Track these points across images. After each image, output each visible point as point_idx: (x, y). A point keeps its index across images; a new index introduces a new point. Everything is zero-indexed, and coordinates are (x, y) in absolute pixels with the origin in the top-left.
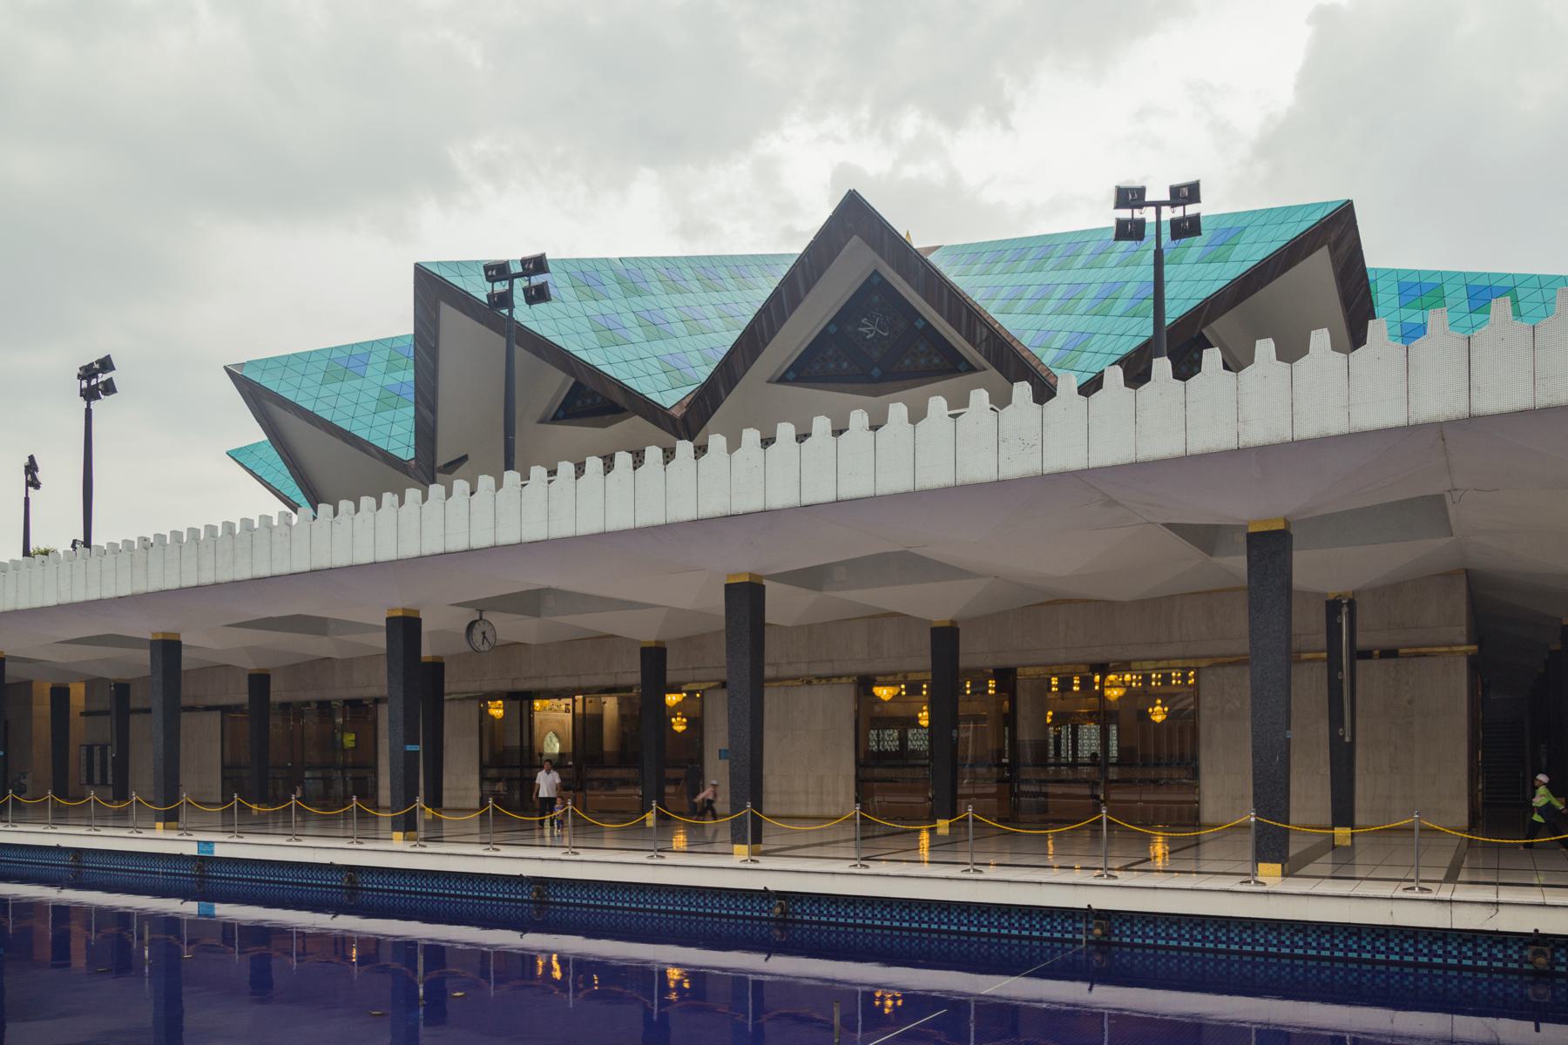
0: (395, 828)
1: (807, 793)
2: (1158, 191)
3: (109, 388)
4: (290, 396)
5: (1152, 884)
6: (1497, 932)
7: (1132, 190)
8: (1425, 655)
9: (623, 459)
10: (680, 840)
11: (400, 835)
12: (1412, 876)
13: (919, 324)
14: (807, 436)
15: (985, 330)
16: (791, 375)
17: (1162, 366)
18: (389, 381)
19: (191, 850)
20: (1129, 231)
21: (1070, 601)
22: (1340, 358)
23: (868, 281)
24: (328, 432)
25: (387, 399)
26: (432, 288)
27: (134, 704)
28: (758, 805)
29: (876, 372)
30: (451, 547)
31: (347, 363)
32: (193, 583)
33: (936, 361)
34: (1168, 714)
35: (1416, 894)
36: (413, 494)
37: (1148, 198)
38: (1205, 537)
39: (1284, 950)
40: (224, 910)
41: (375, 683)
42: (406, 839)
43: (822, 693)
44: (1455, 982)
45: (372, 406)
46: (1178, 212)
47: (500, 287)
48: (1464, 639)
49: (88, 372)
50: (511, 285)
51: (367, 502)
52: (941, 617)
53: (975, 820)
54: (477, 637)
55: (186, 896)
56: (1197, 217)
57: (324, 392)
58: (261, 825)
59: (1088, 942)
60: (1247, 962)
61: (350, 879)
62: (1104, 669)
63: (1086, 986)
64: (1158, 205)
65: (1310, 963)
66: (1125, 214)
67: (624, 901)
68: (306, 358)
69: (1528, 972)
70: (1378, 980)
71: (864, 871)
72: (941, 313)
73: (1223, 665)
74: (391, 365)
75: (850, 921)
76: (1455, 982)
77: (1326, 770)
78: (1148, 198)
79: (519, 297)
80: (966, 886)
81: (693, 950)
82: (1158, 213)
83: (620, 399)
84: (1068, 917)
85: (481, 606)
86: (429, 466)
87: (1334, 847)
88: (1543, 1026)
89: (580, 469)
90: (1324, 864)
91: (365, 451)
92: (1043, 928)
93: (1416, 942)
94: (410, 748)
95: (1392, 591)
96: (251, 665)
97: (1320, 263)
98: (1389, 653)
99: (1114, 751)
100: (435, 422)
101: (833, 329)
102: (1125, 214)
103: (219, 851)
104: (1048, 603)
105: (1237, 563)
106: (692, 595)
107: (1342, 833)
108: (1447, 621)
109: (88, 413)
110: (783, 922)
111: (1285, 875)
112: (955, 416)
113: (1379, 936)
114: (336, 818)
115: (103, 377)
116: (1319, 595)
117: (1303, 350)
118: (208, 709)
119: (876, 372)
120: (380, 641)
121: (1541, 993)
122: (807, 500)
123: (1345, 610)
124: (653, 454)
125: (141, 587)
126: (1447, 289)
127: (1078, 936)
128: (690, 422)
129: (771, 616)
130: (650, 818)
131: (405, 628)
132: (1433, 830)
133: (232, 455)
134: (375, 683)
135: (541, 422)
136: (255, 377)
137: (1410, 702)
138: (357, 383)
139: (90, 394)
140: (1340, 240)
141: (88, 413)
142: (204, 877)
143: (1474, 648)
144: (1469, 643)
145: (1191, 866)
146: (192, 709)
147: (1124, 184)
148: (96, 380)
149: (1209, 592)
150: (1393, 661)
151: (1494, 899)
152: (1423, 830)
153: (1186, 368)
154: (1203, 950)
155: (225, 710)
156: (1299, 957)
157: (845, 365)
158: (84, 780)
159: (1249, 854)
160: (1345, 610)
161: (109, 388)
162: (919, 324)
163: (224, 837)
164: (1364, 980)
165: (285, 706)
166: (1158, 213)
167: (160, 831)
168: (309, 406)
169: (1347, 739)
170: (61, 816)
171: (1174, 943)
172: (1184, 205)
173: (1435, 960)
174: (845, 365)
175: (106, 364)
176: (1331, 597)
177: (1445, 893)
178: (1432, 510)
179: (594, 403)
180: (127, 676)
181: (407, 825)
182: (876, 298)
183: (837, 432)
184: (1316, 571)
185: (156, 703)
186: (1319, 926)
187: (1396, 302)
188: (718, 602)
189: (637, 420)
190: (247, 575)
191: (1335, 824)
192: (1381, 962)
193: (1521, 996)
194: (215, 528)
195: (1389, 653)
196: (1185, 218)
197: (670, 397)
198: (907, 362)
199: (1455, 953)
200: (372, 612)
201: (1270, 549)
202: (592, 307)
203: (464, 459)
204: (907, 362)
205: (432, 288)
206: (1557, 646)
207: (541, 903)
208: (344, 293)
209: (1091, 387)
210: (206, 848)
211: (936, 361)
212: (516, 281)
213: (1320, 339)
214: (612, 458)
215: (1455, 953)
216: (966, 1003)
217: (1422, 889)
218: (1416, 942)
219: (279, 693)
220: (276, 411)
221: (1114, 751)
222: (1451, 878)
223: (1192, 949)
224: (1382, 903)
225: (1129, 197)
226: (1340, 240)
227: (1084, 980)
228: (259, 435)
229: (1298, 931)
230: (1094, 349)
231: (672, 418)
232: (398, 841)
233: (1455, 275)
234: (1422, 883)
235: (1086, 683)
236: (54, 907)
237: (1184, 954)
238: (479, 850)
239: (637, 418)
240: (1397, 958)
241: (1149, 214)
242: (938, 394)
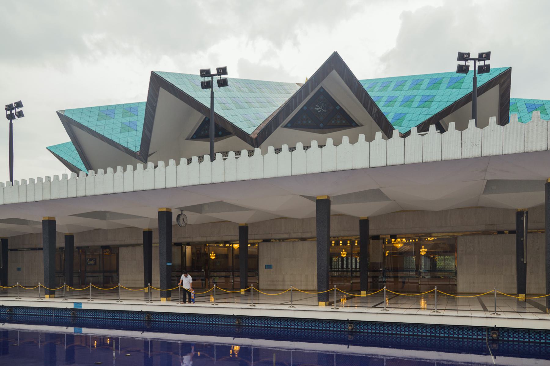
0: (162, 296)
1: (301, 281)
2: (474, 55)
3: (20, 115)
4: (85, 124)
5: (376, 312)
7: (466, 54)
9: (232, 154)
10: (343, 301)
11: (48, 296)
12: (435, 308)
13: (338, 108)
14: (308, 147)
15: (376, 110)
16: (289, 125)
17: (433, 127)
18: (135, 117)
19: (71, 306)
20: (462, 70)
21: (407, 211)
22: (500, 127)
24: (102, 139)
26: (157, 82)
29: (321, 125)
30: (203, 182)
32: (208, 181)
33: (344, 122)
34: (216, 256)
35: (495, 316)
36: (140, 166)
37: (471, 57)
39: (428, 334)
40: (85, 331)
42: (167, 300)
43: (306, 244)
44: (522, 347)
46: (482, 63)
47: (207, 79)
49: (9, 108)
50: (212, 79)
51: (119, 168)
52: (520, 206)
53: (337, 290)
54: (181, 221)
55: (68, 325)
56: (489, 66)
57: (99, 123)
59: (489, 340)
60: (433, 340)
61: (73, 313)
62: (394, 237)
63: (232, 338)
64: (475, 60)
65: (474, 341)
66: (463, 63)
67: (167, 319)
68: (90, 110)
69: (346, 331)
70: (515, 347)
71: (254, 307)
72: (361, 102)
73: (467, 235)
75: (279, 326)
76: (527, 347)
77: (143, 273)
78: (471, 57)
79: (215, 84)
81: (58, 327)
82: (475, 63)
83: (230, 130)
84: (342, 323)
85: (182, 209)
86: (144, 155)
88: (350, 346)
89: (189, 161)
91: (117, 148)
92: (364, 329)
93: (540, 335)
96: (67, 232)
97: (495, 91)
99: (358, 267)
100: (151, 137)
101: (305, 108)
102: (463, 63)
103: (84, 307)
104: (398, 212)
106: (148, 216)
107: (522, 297)
109: (11, 125)
110: (239, 326)
111: (326, 305)
112: (237, 158)
115: (18, 110)
116: (357, 218)
117: (466, 127)
119: (321, 125)
121: (350, 337)
122: (371, 166)
123: (525, 215)
124: (244, 152)
125: (47, 197)
126: (518, 105)
127: (484, 337)
128: (256, 141)
130: (243, 291)
131: (50, 224)
132: (500, 294)
133: (49, 149)
135: (187, 139)
136: (70, 116)
137: (538, 249)
138: (112, 121)
139: (10, 117)
140: (504, 82)
141: (11, 125)
142: (76, 317)
146: (11, 250)
147: (462, 51)
148: (14, 111)
149: (461, 209)
152: (497, 294)
153: (442, 129)
154: (376, 333)
156: (433, 336)
157: (310, 122)
159: (316, 299)
160: (525, 215)
161: (20, 115)
162: (338, 108)
163: (86, 301)
164: (542, 349)
165: (78, 248)
166: (475, 63)
167: (47, 298)
168: (94, 129)
169: (525, 262)
171: (424, 334)
172: (484, 60)
173: (479, 337)
175: (19, 104)
176: (519, 211)
179: (213, 131)
182: (322, 97)
183: (321, 146)
186: (458, 327)
188: (156, 216)
189: (235, 138)
190: (102, 192)
192: (480, 339)
193: (468, 345)
194: (34, 180)
196: (484, 66)
197: (250, 130)
198: (333, 122)
200: (39, 216)
201: (323, 205)
205: (157, 82)
207: (75, 317)
208: (116, 81)
209: (405, 135)
210: (78, 305)
211: (344, 122)
212: (214, 77)
213: (493, 120)
214: (227, 153)
216: (213, 346)
217: (497, 314)
218: (540, 335)
219: (77, 243)
220: (79, 132)
221: (358, 267)
223: (396, 334)
224: (482, 319)
225: (463, 56)
226: (504, 82)
227: (232, 337)
228: (67, 139)
229: (479, 330)
230: (409, 119)
231: (251, 138)
232: (163, 301)
233: (521, 100)
235: (390, 242)
236: (67, 335)
237: (419, 337)
238: (144, 303)
239: (235, 137)
240: (522, 340)
241: (471, 63)
242: (330, 137)
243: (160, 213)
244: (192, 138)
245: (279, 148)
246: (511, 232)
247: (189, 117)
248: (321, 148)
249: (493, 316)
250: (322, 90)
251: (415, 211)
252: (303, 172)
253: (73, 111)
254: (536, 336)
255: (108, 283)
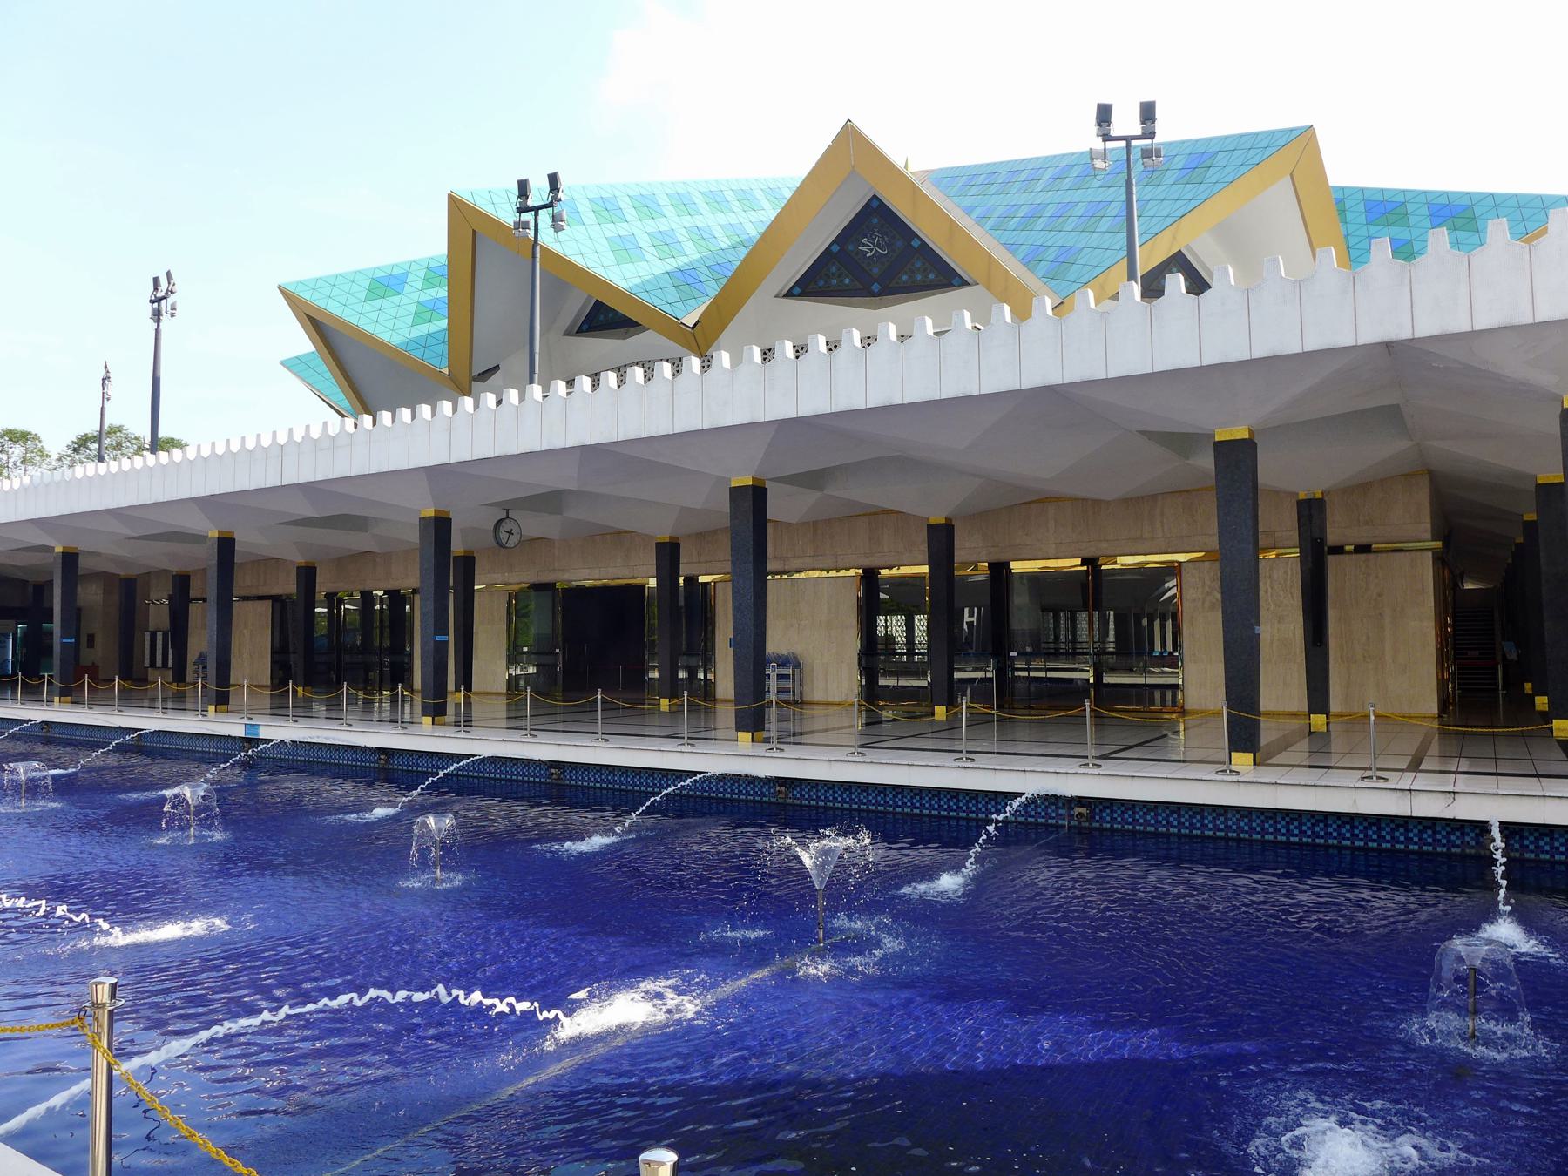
6: (1454, 820)
8: (1401, 550)
16: (797, 290)
23: (868, 205)
25: (424, 311)
27: (192, 594)
28: (468, 688)
31: (385, 285)
38: (1181, 442)
41: (408, 578)
45: (409, 320)
48: (1428, 535)
57: (367, 307)
58: (304, 710)
74: (428, 282)
80: (955, 773)
85: (507, 508)
86: (468, 374)
87: (1311, 733)
90: (1300, 752)
94: (438, 638)
95: (1361, 489)
96: (300, 560)
98: (1363, 549)
101: (836, 248)
105: (1206, 462)
107: (1318, 720)
108: (1412, 521)
113: (1398, 826)
114: (1531, 735)
118: (260, 598)
120: (413, 537)
126: (1410, 208)
128: (700, 340)
129: (772, 513)
131: (440, 527)
133: (282, 363)
134: (408, 578)
135: (567, 333)
136: (306, 295)
138: (396, 299)
143: (1438, 544)
144: (1433, 540)
145: (944, 745)
150: (1363, 556)
151: (1451, 789)
155: (275, 599)
157: (847, 281)
158: (147, 664)
170: (127, 700)
174: (847, 281)
177: (1407, 781)
178: (1392, 416)
179: (606, 318)
180: (133, 572)
181: (436, 710)
184: (1285, 472)
185: (212, 593)
187: (1363, 219)
188: (725, 505)
191: (1312, 710)
195: (1363, 549)
198: (905, 278)
199: (1532, 847)
201: (1237, 459)
202: (610, 230)
203: (497, 368)
204: (905, 278)
206: (1520, 540)
211: (931, 276)
215: (1532, 847)
222: (1415, 766)
224: (1265, 788)
234: (1380, 774)
243: (736, 492)
244: (580, 331)
245: (800, 343)
246: (1338, 550)
247: (516, 293)
248: (1528, 241)
249: (1366, 784)
250: (875, 204)
251: (1077, 499)
252: (1191, 361)
253: (315, 284)
254: (1541, 843)
255: (1133, 712)
